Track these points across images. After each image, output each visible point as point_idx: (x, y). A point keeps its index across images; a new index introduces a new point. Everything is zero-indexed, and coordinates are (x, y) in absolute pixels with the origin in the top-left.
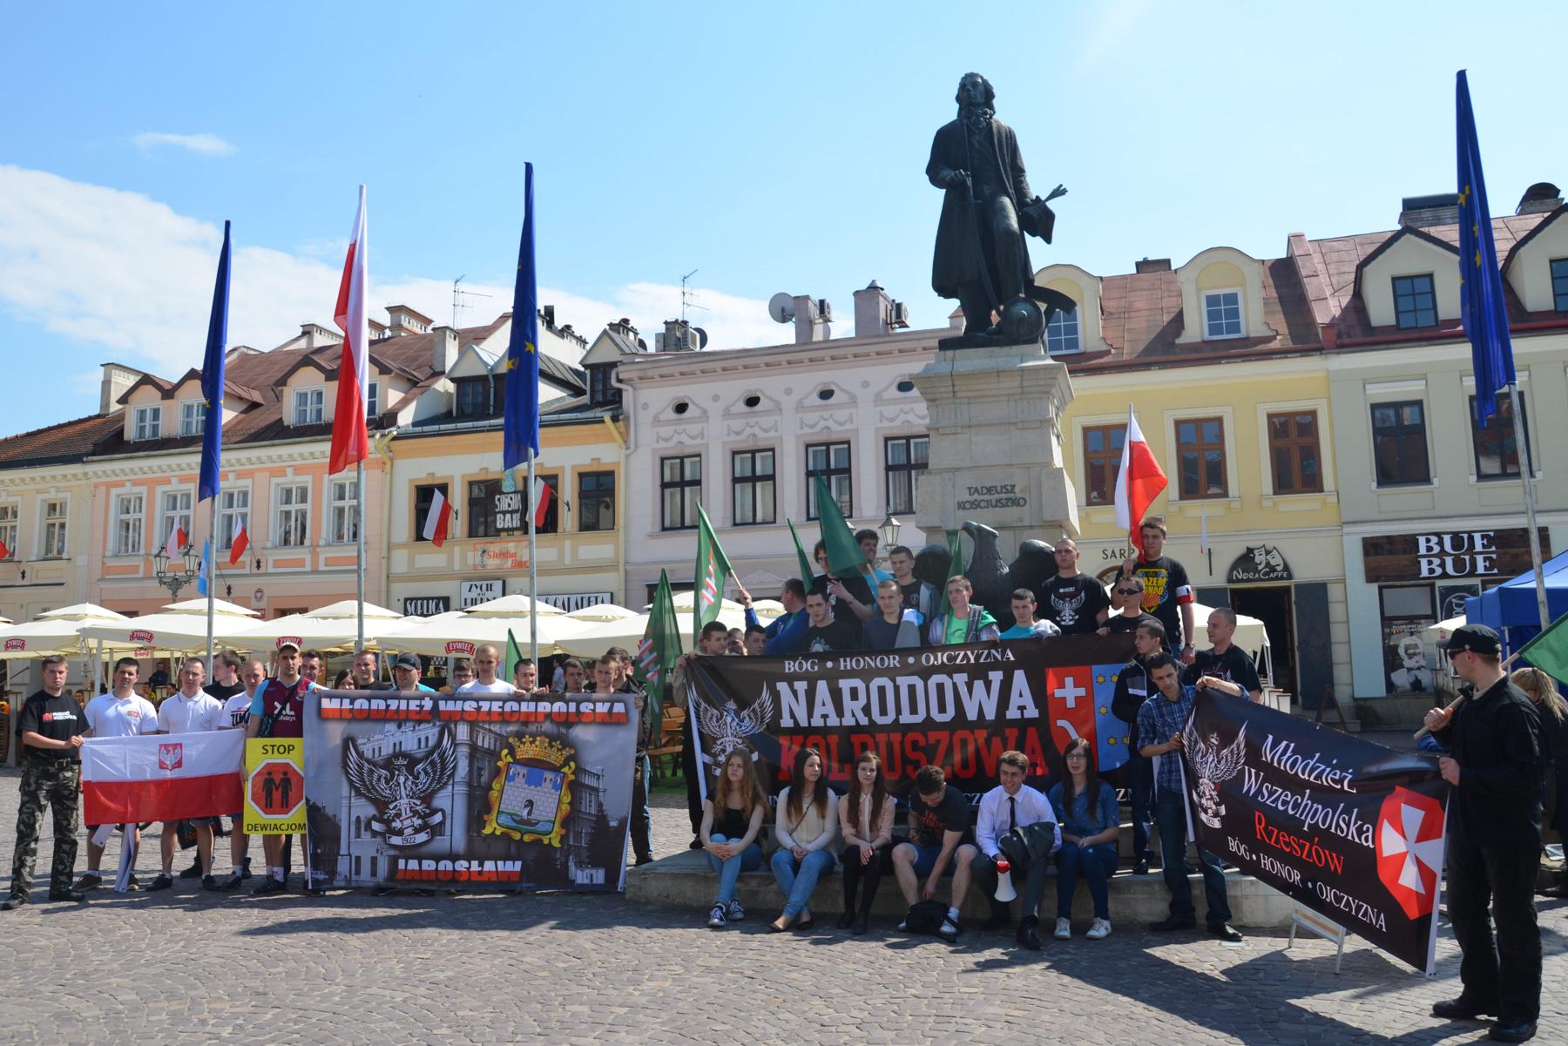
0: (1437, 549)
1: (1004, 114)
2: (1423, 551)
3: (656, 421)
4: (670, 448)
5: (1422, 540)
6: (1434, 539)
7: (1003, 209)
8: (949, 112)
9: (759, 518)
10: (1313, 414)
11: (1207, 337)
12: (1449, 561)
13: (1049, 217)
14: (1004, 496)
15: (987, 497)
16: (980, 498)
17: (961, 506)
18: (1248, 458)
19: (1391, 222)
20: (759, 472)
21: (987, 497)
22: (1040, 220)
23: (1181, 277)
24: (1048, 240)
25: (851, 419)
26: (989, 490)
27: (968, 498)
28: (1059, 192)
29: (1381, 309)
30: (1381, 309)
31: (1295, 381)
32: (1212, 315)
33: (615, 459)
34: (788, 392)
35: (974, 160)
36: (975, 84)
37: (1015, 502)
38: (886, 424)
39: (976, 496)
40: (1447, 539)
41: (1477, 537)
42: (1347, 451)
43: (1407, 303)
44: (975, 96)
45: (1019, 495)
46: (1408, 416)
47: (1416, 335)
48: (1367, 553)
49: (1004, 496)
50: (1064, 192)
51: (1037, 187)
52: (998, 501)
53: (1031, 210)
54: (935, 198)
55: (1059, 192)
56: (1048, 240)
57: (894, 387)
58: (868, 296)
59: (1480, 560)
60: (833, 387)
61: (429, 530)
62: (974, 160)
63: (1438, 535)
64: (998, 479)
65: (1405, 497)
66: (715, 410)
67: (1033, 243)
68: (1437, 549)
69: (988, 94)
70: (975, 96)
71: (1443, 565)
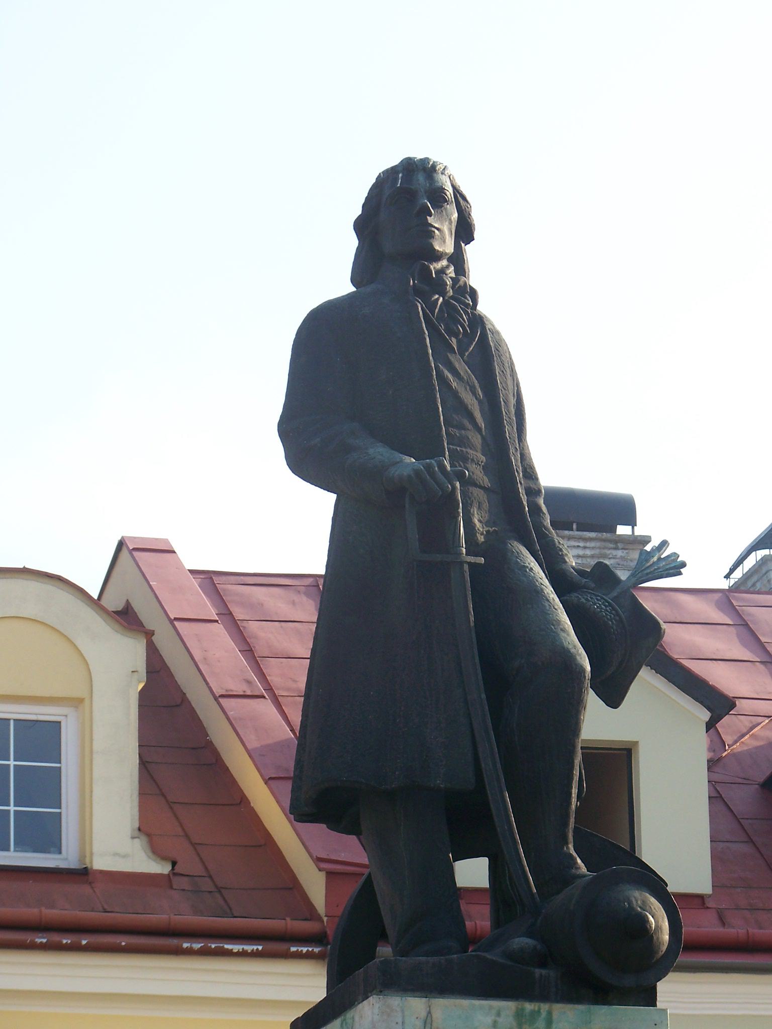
1: (502, 280)
35: (396, 360)
44: (407, 216)
62: (396, 360)
67: (593, 702)
70: (407, 216)
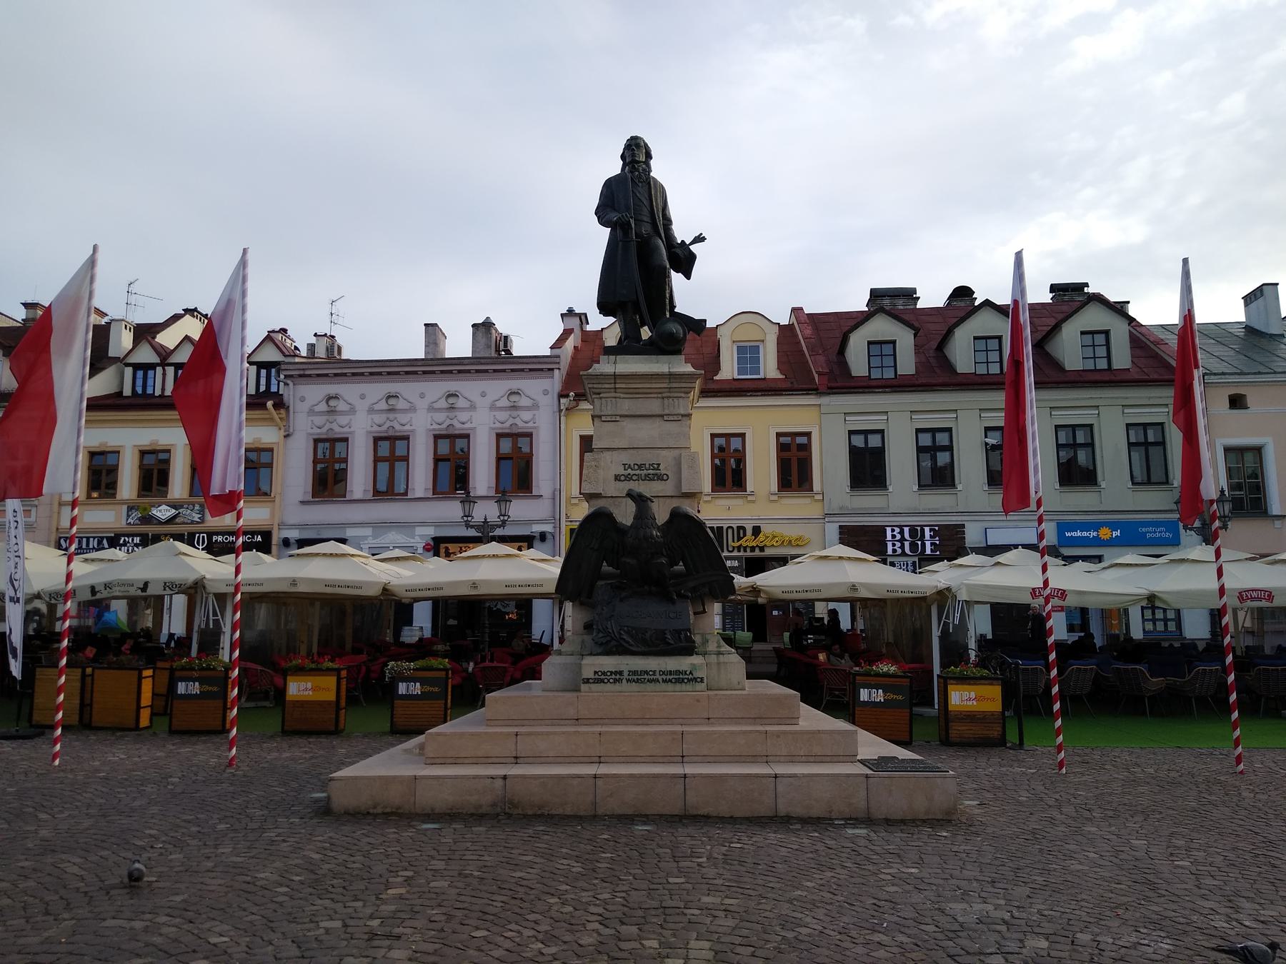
0: (898, 537)
1: (658, 171)
2: (889, 537)
3: (311, 412)
4: (322, 433)
5: (889, 530)
6: (897, 530)
7: (657, 248)
8: (614, 167)
10: (808, 435)
11: (736, 376)
12: (907, 544)
13: (692, 258)
16: (632, 472)
18: (762, 467)
19: (859, 303)
22: (684, 260)
23: (720, 332)
24: (688, 277)
25: (470, 421)
26: (640, 467)
27: (621, 471)
28: (699, 239)
30: (857, 359)
31: (795, 414)
32: (740, 360)
33: (274, 440)
34: (422, 396)
35: (633, 206)
36: (638, 146)
37: (660, 478)
38: (498, 425)
39: (629, 471)
40: (906, 530)
41: (927, 530)
42: (830, 464)
43: (876, 362)
44: (636, 154)
45: (663, 472)
47: (55, 515)
48: (841, 533)
51: (682, 232)
53: (678, 251)
54: (603, 234)
55: (699, 239)
56: (688, 277)
58: (484, 329)
59: (928, 544)
62: (633, 206)
63: (901, 527)
65: (869, 500)
67: (676, 278)
68: (898, 537)
70: (636, 154)
71: (902, 547)
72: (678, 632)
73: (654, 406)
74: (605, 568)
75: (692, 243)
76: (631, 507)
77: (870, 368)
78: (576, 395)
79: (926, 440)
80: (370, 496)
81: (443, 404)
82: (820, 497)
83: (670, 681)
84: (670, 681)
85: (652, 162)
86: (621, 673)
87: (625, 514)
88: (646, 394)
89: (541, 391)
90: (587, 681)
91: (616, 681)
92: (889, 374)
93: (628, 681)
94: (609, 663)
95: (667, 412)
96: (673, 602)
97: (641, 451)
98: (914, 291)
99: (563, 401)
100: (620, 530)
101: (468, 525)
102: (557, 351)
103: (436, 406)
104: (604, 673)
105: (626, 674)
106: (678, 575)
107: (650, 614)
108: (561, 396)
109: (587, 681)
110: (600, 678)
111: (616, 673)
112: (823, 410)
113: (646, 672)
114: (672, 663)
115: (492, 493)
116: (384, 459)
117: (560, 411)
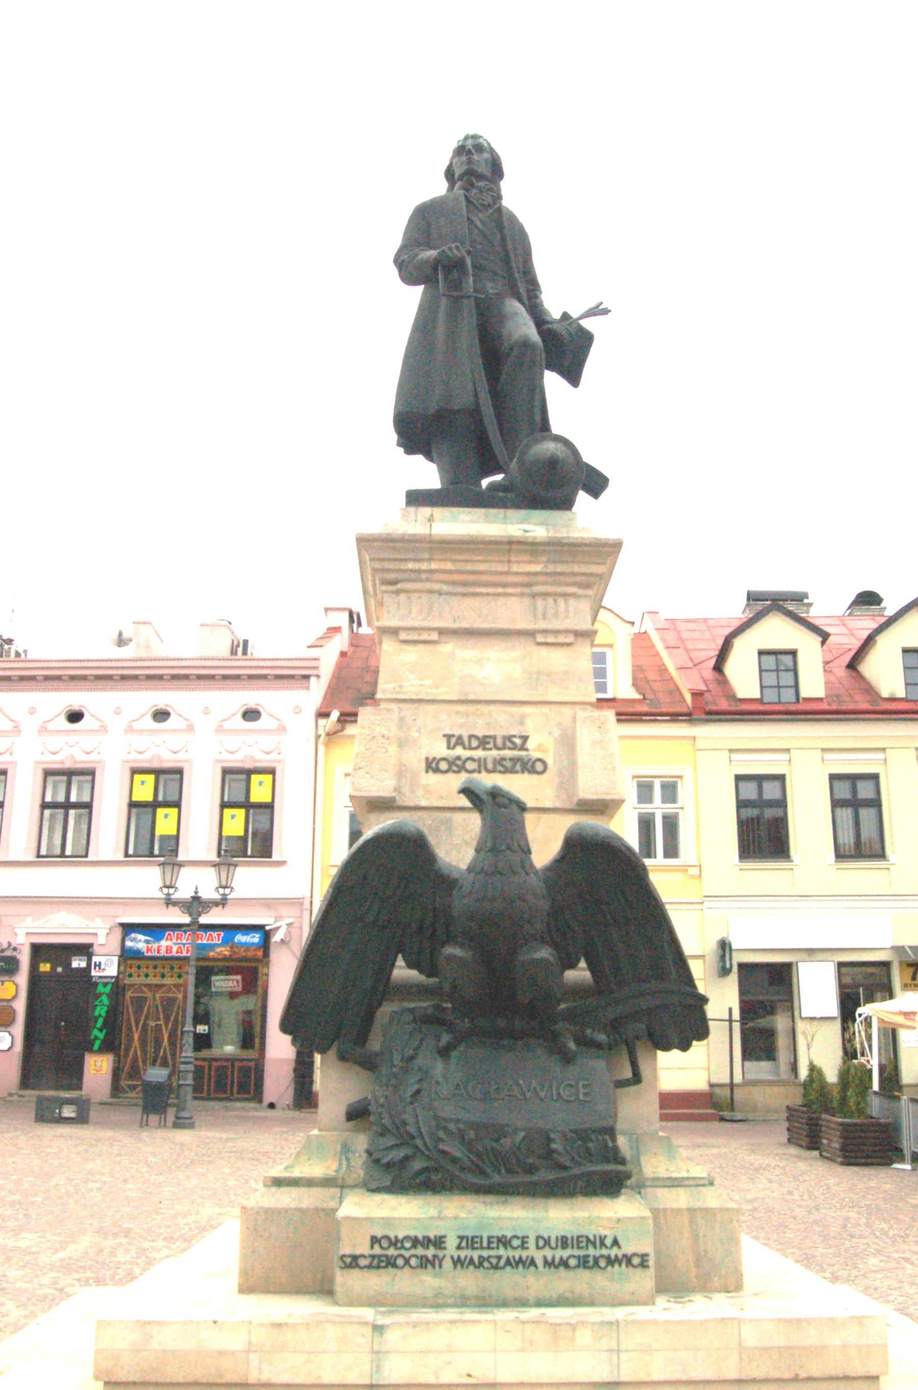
1: (514, 196)
9: (68, 852)
13: (585, 340)
14: (507, 753)
15: (479, 753)
17: (432, 766)
19: (735, 609)
20: (73, 798)
21: (479, 753)
22: (568, 349)
26: (484, 742)
27: (441, 750)
28: (598, 311)
29: (744, 678)
30: (744, 678)
37: (530, 766)
39: (459, 751)
43: (770, 679)
44: (476, 170)
45: (535, 755)
46: (771, 791)
49: (507, 753)
50: (606, 312)
51: (556, 302)
52: (500, 761)
57: (239, 716)
60: (169, 709)
61: (144, 1123)
64: (500, 722)
66: (29, 726)
67: (552, 381)
69: (496, 170)
70: (476, 170)
72: (582, 1135)
73: (511, 612)
74: (402, 971)
75: (581, 317)
76: (473, 823)
77: (762, 687)
78: (342, 714)
79: (844, 791)
80: (31, 857)
81: (149, 722)
82: (695, 871)
83: (564, 1263)
84: (564, 1263)
85: (503, 184)
86: (439, 1242)
87: (457, 846)
88: (500, 586)
89: (294, 712)
90: (352, 1263)
91: (425, 1263)
92: (788, 696)
93: (458, 1262)
94: (407, 1212)
95: (542, 625)
96: (568, 1059)
97: (485, 709)
98: (806, 596)
99: (322, 722)
100: (445, 882)
101: (169, 902)
102: (314, 653)
103: (136, 726)
104: (395, 1243)
105: (451, 1243)
106: (577, 991)
107: (536, 1095)
108: (323, 714)
109: (352, 1263)
110: (388, 1253)
111: (427, 1242)
112: (699, 744)
113: (504, 1242)
114: (560, 1217)
115: (213, 857)
116: (54, 806)
117: (318, 737)
